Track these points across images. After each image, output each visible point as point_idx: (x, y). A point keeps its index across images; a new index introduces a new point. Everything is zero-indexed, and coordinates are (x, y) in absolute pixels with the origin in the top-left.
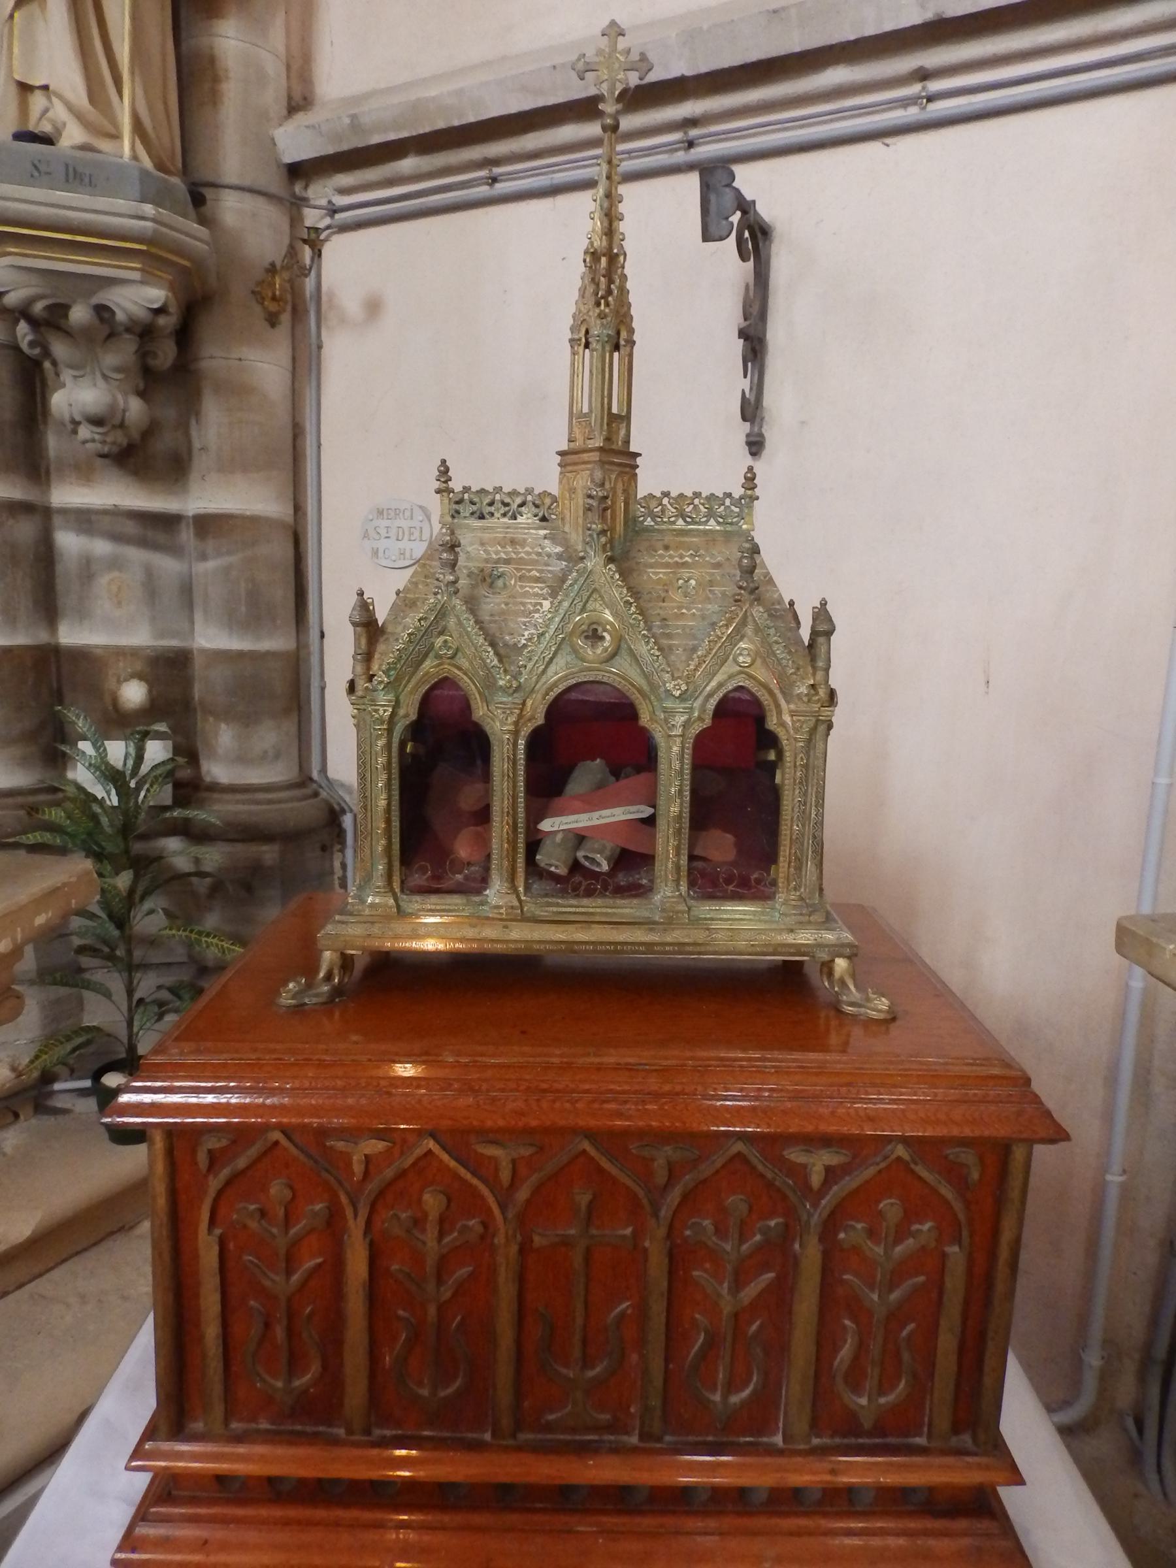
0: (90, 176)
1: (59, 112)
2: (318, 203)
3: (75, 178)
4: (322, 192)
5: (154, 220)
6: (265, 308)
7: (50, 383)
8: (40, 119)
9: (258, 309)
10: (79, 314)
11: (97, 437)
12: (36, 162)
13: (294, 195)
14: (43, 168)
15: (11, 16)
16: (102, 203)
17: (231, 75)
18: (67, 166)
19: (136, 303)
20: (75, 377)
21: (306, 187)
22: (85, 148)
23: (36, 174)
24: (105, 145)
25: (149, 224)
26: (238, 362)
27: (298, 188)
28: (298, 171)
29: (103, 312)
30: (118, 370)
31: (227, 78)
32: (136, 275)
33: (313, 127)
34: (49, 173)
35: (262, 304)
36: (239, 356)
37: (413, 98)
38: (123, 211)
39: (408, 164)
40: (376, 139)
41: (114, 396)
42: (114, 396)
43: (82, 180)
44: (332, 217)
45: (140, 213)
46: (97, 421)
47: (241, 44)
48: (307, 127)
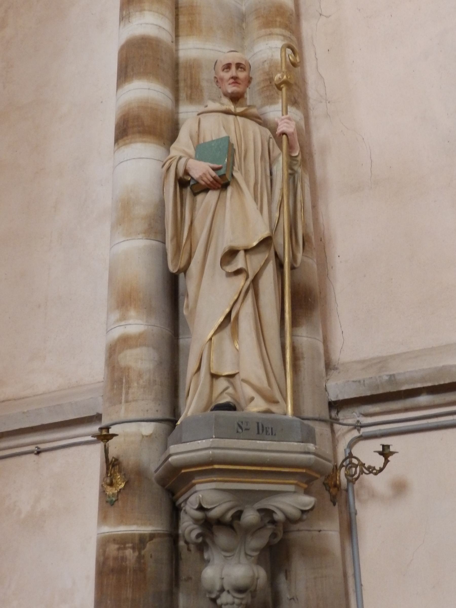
0: (272, 429)
1: (249, 391)
2: (345, 422)
3: (263, 430)
4: (350, 416)
5: (314, 454)
6: (330, 493)
7: (183, 556)
8: (222, 393)
9: (327, 494)
10: (250, 516)
11: (237, 601)
12: (240, 424)
13: (331, 417)
14: (244, 426)
15: (211, 339)
16: (284, 445)
17: (305, 356)
18: (258, 423)
19: (294, 507)
20: (225, 557)
21: (337, 414)
22: (268, 412)
23: (240, 430)
24: (274, 408)
25: (312, 456)
26: (318, 533)
27: (334, 414)
28: (336, 406)
29: (267, 513)
30: (254, 550)
31: (303, 358)
32: (292, 488)
33: (359, 381)
34: (247, 429)
35: (329, 491)
36: (319, 529)
37: (441, 365)
38: (299, 450)
39: (423, 399)
40: (404, 388)
41: (253, 571)
42: (253, 571)
43: (267, 432)
44: (359, 430)
45: (307, 450)
46: (240, 590)
47: (309, 339)
48: (353, 381)
